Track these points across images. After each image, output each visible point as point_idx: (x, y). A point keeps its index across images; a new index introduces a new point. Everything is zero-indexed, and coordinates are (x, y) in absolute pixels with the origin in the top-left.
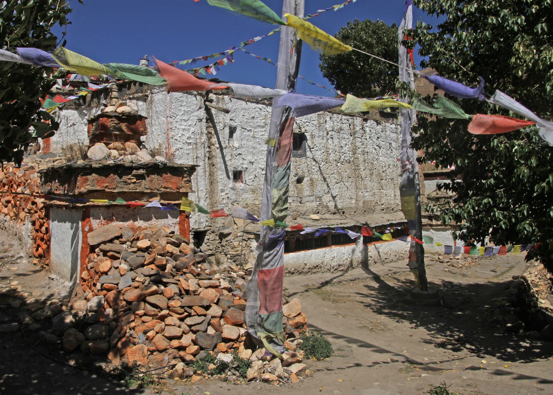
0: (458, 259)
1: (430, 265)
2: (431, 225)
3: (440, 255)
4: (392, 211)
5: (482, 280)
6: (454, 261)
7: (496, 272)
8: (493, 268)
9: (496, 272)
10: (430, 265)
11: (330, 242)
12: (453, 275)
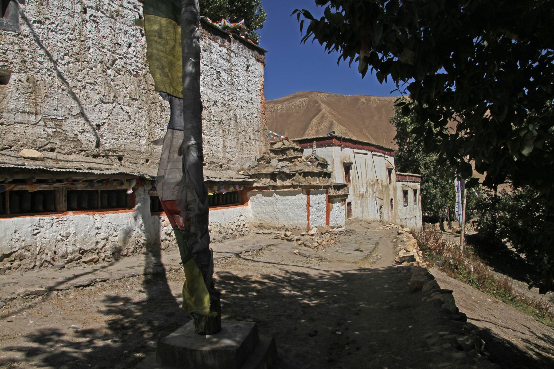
0: (312, 235)
1: (273, 245)
2: (275, 187)
3: (287, 230)
4: (219, 168)
5: (349, 265)
6: (307, 237)
7: (362, 251)
8: (356, 246)
9: (362, 251)
10: (273, 245)
11: (63, 205)
12: (305, 259)
